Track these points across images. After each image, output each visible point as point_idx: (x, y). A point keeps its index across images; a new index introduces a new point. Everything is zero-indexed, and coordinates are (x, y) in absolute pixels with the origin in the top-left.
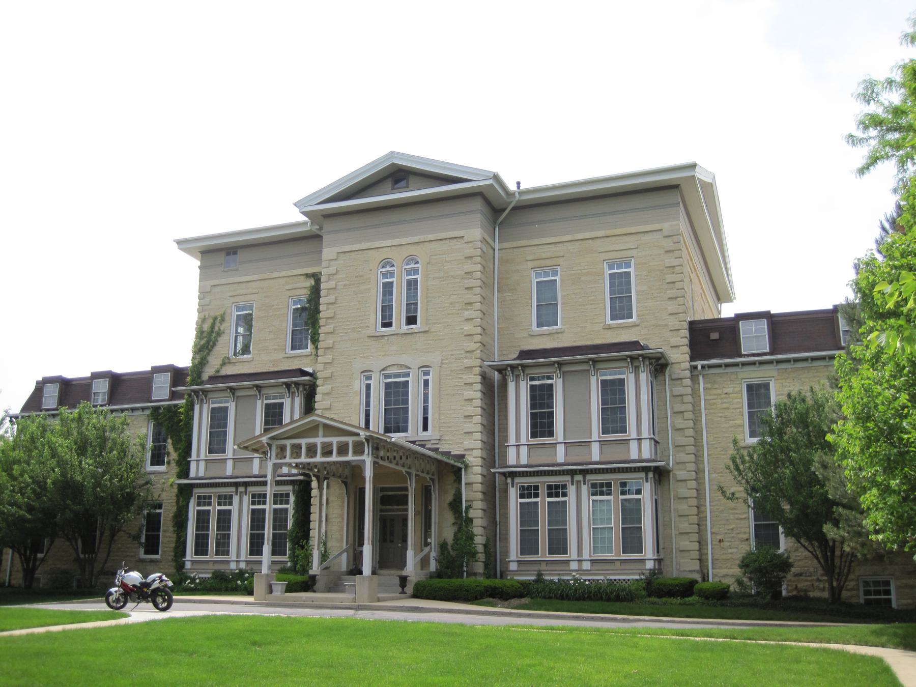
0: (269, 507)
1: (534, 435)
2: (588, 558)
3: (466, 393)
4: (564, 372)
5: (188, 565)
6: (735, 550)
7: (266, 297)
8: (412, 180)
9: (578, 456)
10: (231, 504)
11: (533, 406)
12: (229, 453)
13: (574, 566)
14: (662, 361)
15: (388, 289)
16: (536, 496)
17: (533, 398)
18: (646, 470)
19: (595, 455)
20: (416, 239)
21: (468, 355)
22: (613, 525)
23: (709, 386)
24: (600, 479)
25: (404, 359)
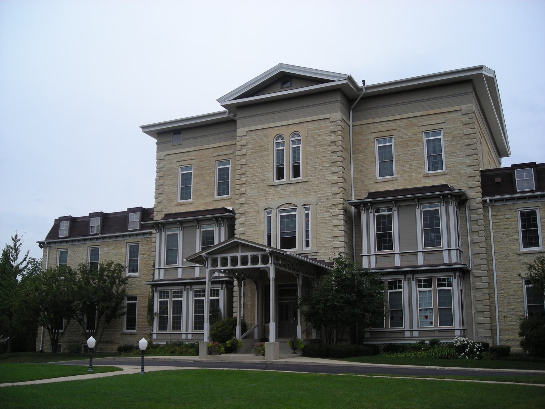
0: (207, 299)
3: (334, 222)
4: (184, 227)
5: (154, 337)
7: (200, 161)
9: (409, 262)
10: (218, 295)
11: (378, 229)
13: (407, 334)
15: (280, 154)
16: (430, 286)
17: (378, 224)
19: (420, 262)
21: (334, 196)
24: (424, 276)
25: (293, 200)
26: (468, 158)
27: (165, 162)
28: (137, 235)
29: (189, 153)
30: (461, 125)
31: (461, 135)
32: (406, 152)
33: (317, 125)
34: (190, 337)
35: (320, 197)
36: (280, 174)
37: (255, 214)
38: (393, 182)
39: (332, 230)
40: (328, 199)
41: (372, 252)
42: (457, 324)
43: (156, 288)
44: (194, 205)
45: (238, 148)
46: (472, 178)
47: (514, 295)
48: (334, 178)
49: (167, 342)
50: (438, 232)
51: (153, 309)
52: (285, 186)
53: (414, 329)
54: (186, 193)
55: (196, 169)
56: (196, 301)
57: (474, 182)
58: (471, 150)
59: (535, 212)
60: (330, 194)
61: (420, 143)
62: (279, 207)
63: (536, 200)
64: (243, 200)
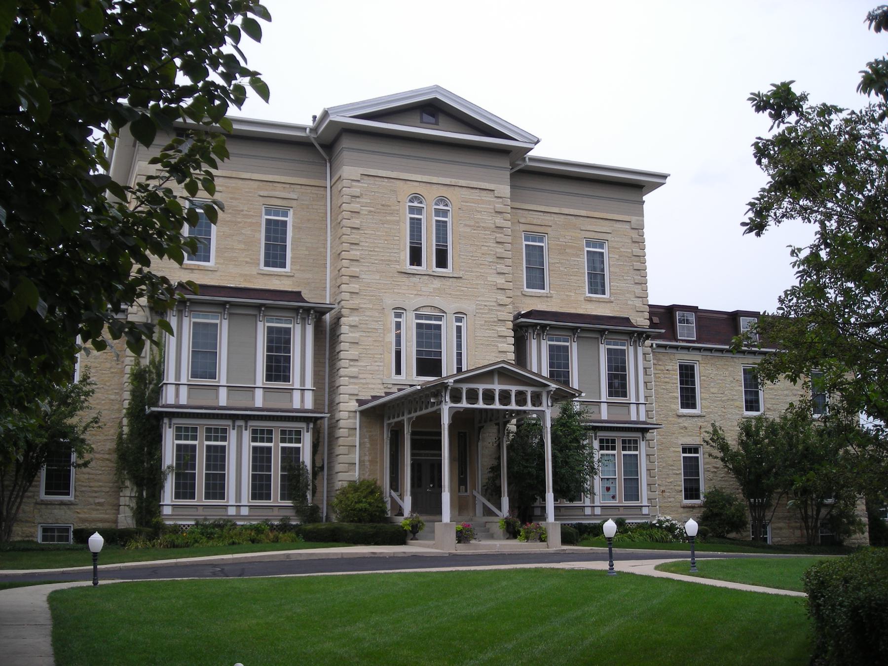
0: (276, 446)
1: (269, 378)
2: (169, 503)
6: (672, 499)
7: (231, 198)
8: (442, 119)
9: (241, 401)
11: (269, 349)
12: (222, 379)
13: (588, 511)
15: (416, 226)
16: (613, 448)
17: (270, 340)
19: (259, 402)
20: (447, 181)
26: (637, 286)
30: (630, 241)
33: (475, 195)
34: (245, 511)
35: (481, 305)
36: (416, 257)
37: (377, 314)
41: (184, 380)
44: (218, 274)
46: (640, 314)
48: (501, 281)
51: (160, 459)
52: (426, 277)
53: (596, 504)
56: (179, 447)
59: (693, 366)
60: (494, 304)
63: (697, 353)
64: (355, 286)
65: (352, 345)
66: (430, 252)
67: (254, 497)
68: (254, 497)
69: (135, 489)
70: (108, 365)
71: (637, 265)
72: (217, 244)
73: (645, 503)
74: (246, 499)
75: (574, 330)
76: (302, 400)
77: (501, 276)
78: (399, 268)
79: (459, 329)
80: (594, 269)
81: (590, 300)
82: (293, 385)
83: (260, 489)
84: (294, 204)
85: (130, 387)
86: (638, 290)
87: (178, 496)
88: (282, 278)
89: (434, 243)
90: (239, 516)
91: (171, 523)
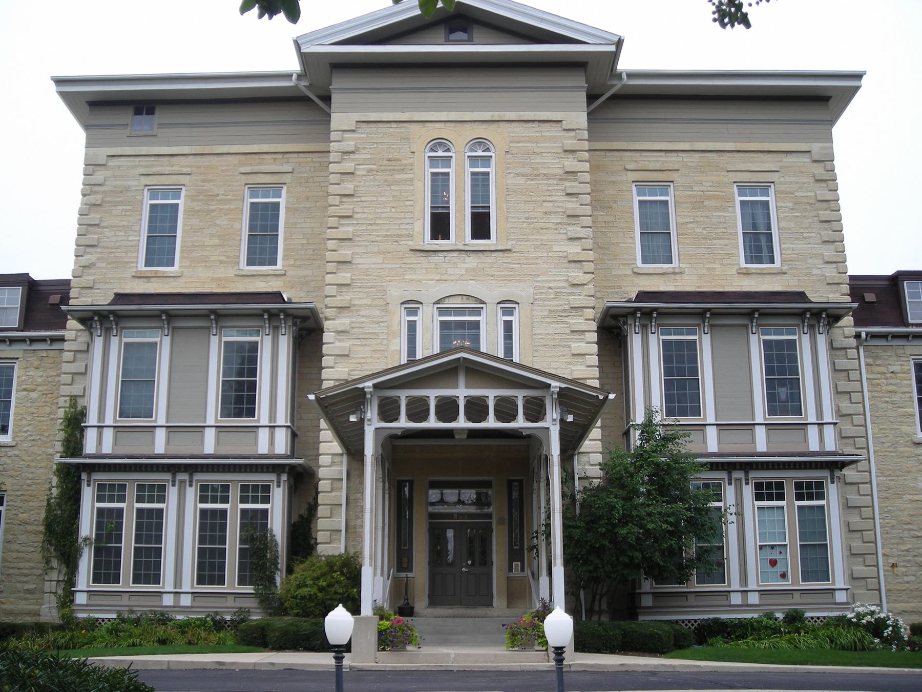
0: (234, 509)
3: (573, 345)
4: (174, 328)
5: (81, 599)
7: (203, 181)
8: (477, 32)
10: (162, 499)
13: (736, 599)
14: (310, 324)
15: (440, 182)
16: (781, 497)
17: (667, 359)
18: (276, 469)
20: (487, 116)
21: (574, 290)
22: (787, 542)
23: (870, 361)
24: (770, 478)
25: (473, 288)
26: (825, 247)
27: (108, 173)
28: (13, 341)
29: (176, 158)
30: (812, 180)
31: (811, 201)
32: (702, 219)
33: (531, 131)
34: (186, 601)
36: (440, 226)
37: (378, 313)
38: (673, 276)
39: (569, 363)
40: (560, 294)
41: (109, 421)
42: (839, 578)
43: (191, 475)
44: (182, 280)
45: (333, 157)
46: (835, 288)
47: (909, 523)
48: (574, 250)
49: (119, 613)
50: (795, 384)
52: (455, 254)
54: (160, 248)
55: (192, 198)
56: (203, 512)
57: (838, 295)
58: (831, 232)
60: (565, 284)
61: (728, 204)
62: (438, 302)
64: (344, 276)
65: (339, 359)
66: (462, 221)
67: (201, 580)
68: (201, 580)
69: (64, 570)
70: (48, 410)
71: (826, 215)
72: (183, 242)
73: (840, 584)
74: (188, 582)
75: (701, 314)
76: (271, 442)
77: (576, 243)
78: (412, 244)
79: (508, 326)
80: (755, 226)
81: (746, 273)
82: (258, 421)
83: (210, 568)
84: (287, 178)
85: (62, 435)
86: (828, 252)
87: (97, 579)
88: (269, 278)
89: (468, 205)
90: (177, 608)
91: (85, 615)
